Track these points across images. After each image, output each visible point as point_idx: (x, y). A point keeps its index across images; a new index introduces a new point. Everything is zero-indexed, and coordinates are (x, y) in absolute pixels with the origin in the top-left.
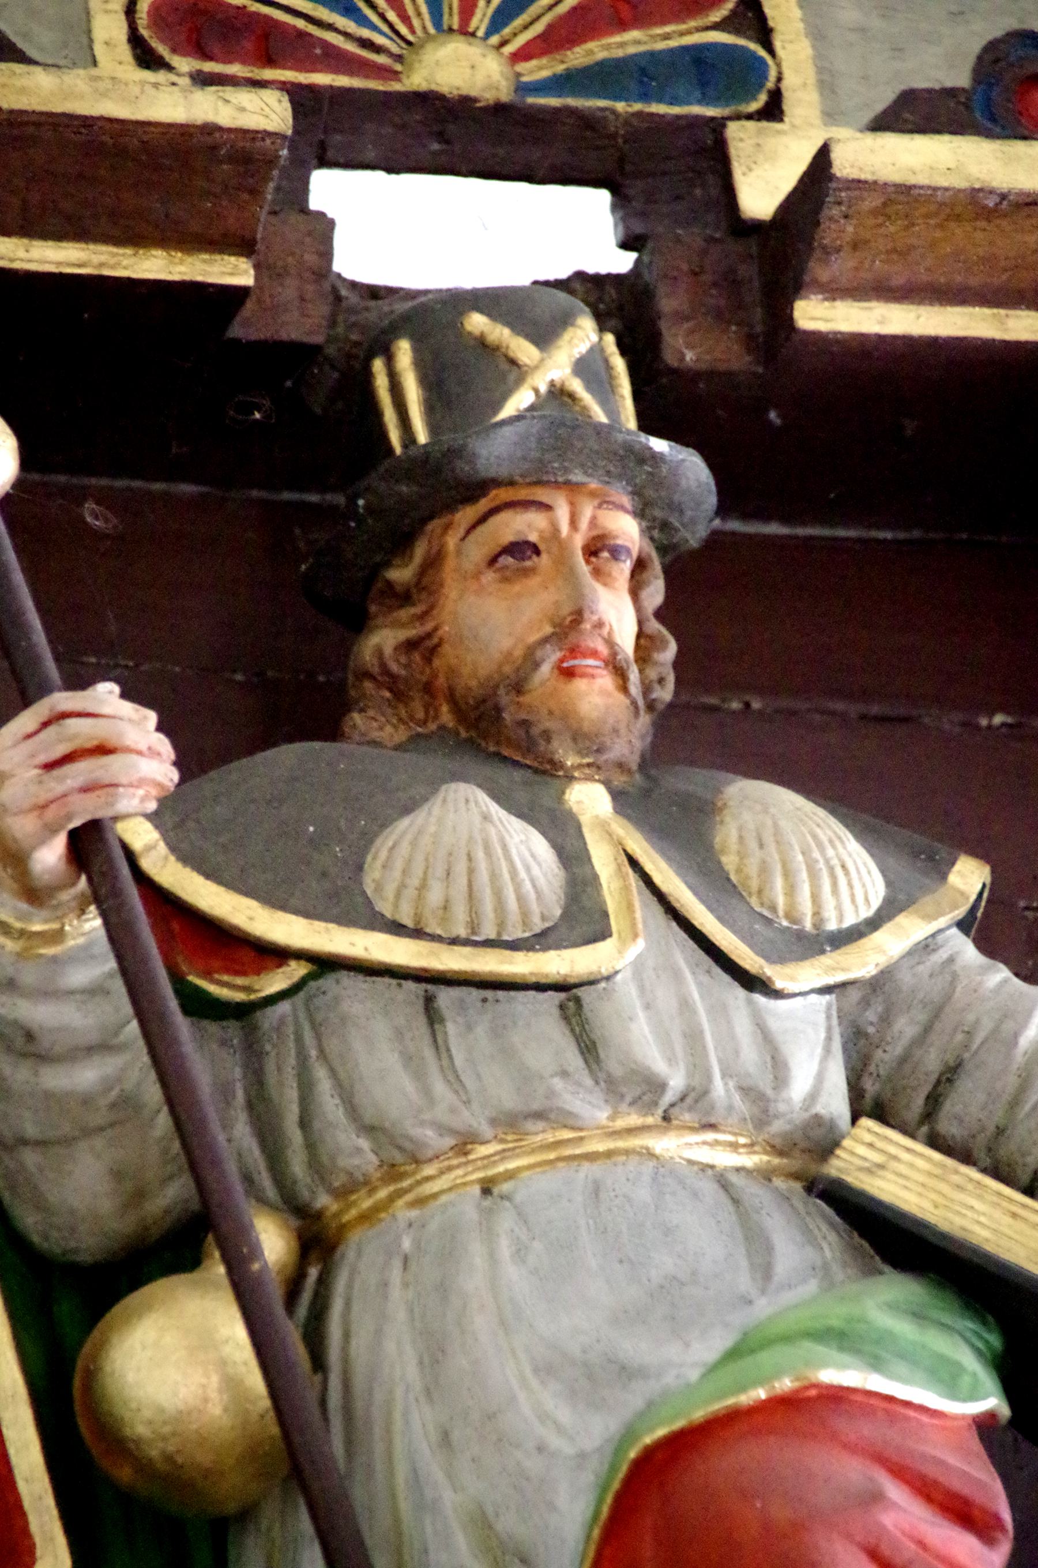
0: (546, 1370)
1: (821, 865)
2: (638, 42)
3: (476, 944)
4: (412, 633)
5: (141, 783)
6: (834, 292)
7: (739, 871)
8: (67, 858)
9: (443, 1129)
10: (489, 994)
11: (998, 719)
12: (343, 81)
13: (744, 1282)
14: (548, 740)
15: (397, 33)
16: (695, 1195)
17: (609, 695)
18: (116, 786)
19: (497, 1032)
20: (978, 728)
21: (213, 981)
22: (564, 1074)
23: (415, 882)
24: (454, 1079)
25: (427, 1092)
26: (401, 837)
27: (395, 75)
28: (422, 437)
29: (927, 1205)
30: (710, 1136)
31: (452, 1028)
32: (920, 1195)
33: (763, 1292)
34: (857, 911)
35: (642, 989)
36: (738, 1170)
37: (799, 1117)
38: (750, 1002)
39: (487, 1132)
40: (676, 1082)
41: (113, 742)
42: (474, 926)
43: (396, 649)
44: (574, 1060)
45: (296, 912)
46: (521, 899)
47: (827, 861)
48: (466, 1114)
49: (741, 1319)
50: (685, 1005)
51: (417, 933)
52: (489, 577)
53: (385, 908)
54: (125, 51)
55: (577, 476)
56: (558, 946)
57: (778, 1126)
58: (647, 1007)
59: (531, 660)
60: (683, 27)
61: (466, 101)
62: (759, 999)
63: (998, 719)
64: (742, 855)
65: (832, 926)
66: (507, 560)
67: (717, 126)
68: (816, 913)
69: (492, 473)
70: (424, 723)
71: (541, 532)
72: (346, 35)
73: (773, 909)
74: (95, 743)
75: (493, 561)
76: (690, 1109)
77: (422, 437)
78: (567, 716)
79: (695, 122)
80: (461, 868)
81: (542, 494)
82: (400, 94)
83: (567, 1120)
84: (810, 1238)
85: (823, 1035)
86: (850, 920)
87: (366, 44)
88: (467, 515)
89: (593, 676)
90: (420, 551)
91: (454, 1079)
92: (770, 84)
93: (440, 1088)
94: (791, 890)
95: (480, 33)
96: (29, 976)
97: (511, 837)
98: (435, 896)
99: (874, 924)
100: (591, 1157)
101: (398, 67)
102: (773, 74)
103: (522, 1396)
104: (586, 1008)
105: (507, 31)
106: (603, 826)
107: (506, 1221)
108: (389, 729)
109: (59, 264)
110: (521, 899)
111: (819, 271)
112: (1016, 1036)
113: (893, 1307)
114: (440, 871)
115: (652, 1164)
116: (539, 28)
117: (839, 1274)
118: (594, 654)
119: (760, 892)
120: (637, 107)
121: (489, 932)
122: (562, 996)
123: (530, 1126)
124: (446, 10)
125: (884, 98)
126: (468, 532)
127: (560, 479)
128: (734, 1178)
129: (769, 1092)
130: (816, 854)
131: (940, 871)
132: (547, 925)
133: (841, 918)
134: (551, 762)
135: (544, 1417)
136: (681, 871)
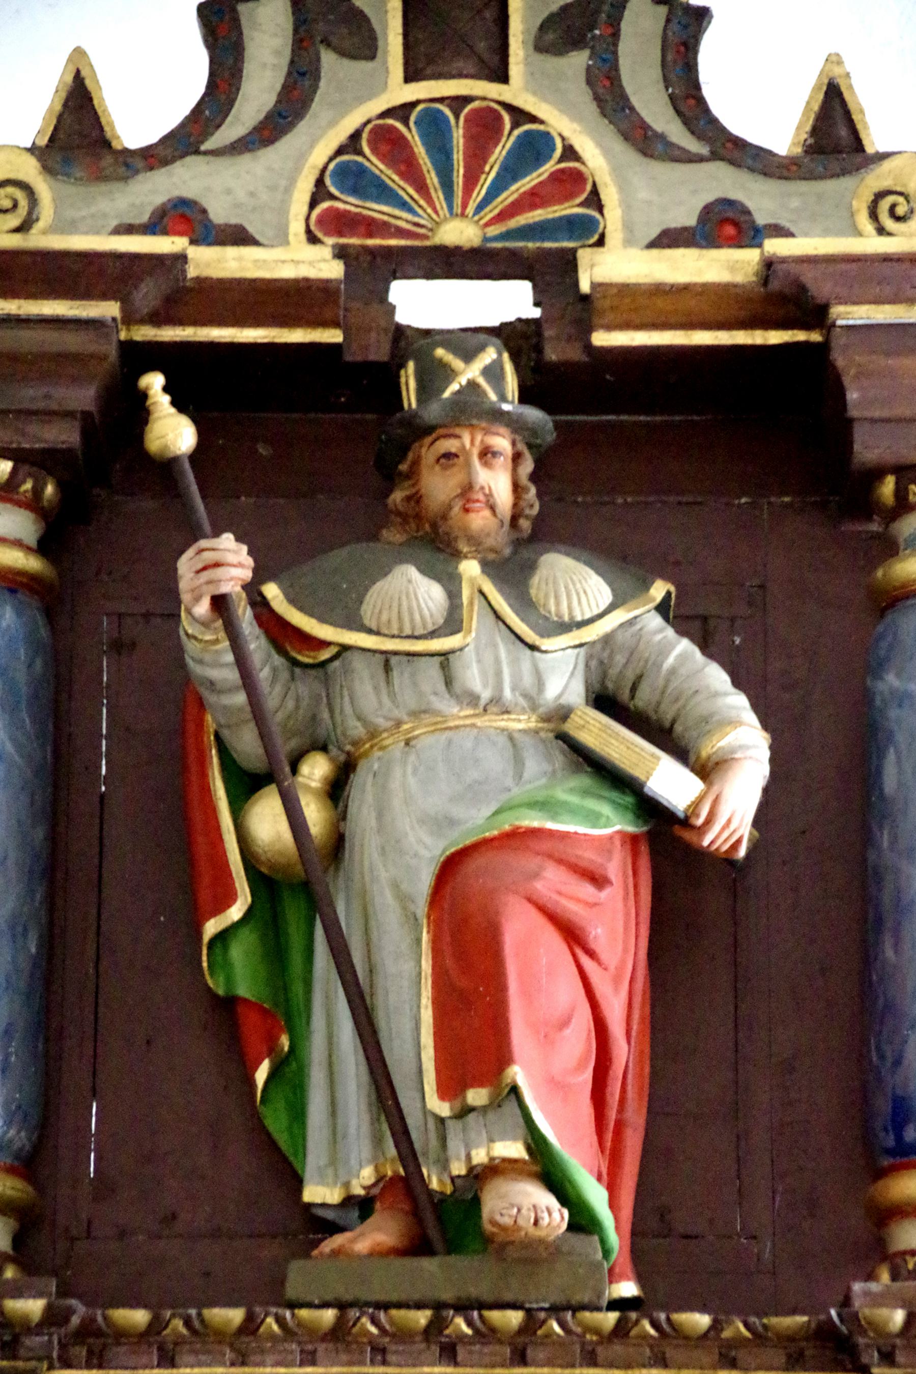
0: (422, 821)
1: (573, 592)
2: (540, 215)
3: (401, 637)
4: (407, 493)
5: (232, 579)
6: (609, 328)
7: (537, 595)
8: (212, 608)
9: (387, 718)
10: (410, 658)
11: (743, 500)
12: (403, 242)
13: (509, 782)
14: (456, 541)
15: (432, 218)
16: (494, 744)
17: (487, 519)
18: (220, 581)
19: (413, 675)
20: (733, 505)
21: (303, 655)
22: (436, 694)
23: (377, 611)
24: (392, 695)
25: (380, 702)
26: (374, 592)
27: (426, 237)
28: (414, 405)
29: (597, 743)
30: (505, 717)
31: (395, 673)
32: (595, 739)
33: (517, 785)
34: (591, 610)
35: (478, 654)
36: (520, 731)
37: (552, 705)
38: (533, 657)
39: (405, 718)
40: (486, 696)
41: (223, 561)
42: (401, 629)
43: (402, 500)
44: (441, 687)
45: (331, 624)
46: (422, 617)
47: (576, 591)
48: (397, 712)
49: (505, 797)
50: (497, 661)
51: (378, 633)
52: (437, 468)
53: (367, 622)
54: (303, 237)
55: (474, 422)
56: (439, 636)
57: (541, 710)
58: (479, 661)
59: (450, 507)
60: (562, 207)
61: (458, 249)
62: (537, 654)
63: (743, 500)
64: (538, 589)
65: (579, 618)
66: (443, 461)
67: (574, 251)
68: (570, 613)
69: (434, 422)
70: (417, 531)
71: (457, 448)
72: (407, 221)
73: (550, 612)
74: (214, 562)
75: (438, 460)
76: (494, 705)
77: (414, 405)
78: (465, 529)
79: (563, 251)
80: (395, 605)
81: (457, 431)
82: (426, 248)
83: (436, 713)
84: (549, 758)
85: (572, 667)
86: (588, 616)
87: (417, 225)
88: (428, 440)
89: (478, 511)
90: (410, 456)
91: (392, 695)
92: (600, 230)
93: (386, 700)
94: (558, 604)
95: (470, 215)
96: (207, 657)
97: (419, 588)
98: (384, 617)
99: (601, 616)
100: (450, 728)
101: (430, 234)
102: (601, 226)
103: (411, 833)
104: (451, 663)
105: (482, 213)
106: (472, 580)
107: (412, 758)
108: (398, 536)
109: (255, 338)
110: (422, 617)
111: (596, 320)
112: (663, 662)
113: (572, 791)
114: (387, 606)
115: (476, 731)
116: (496, 211)
117: (559, 774)
118: (478, 501)
119: (544, 605)
120: (538, 244)
121: (407, 631)
122: (443, 658)
123: (423, 716)
124: (455, 206)
125: (654, 233)
126: (429, 447)
127: (467, 423)
128: (516, 735)
129: (535, 696)
130: (571, 586)
131: (646, 586)
132: (436, 627)
133: (583, 614)
134: (457, 550)
135: (420, 841)
136: (507, 599)
